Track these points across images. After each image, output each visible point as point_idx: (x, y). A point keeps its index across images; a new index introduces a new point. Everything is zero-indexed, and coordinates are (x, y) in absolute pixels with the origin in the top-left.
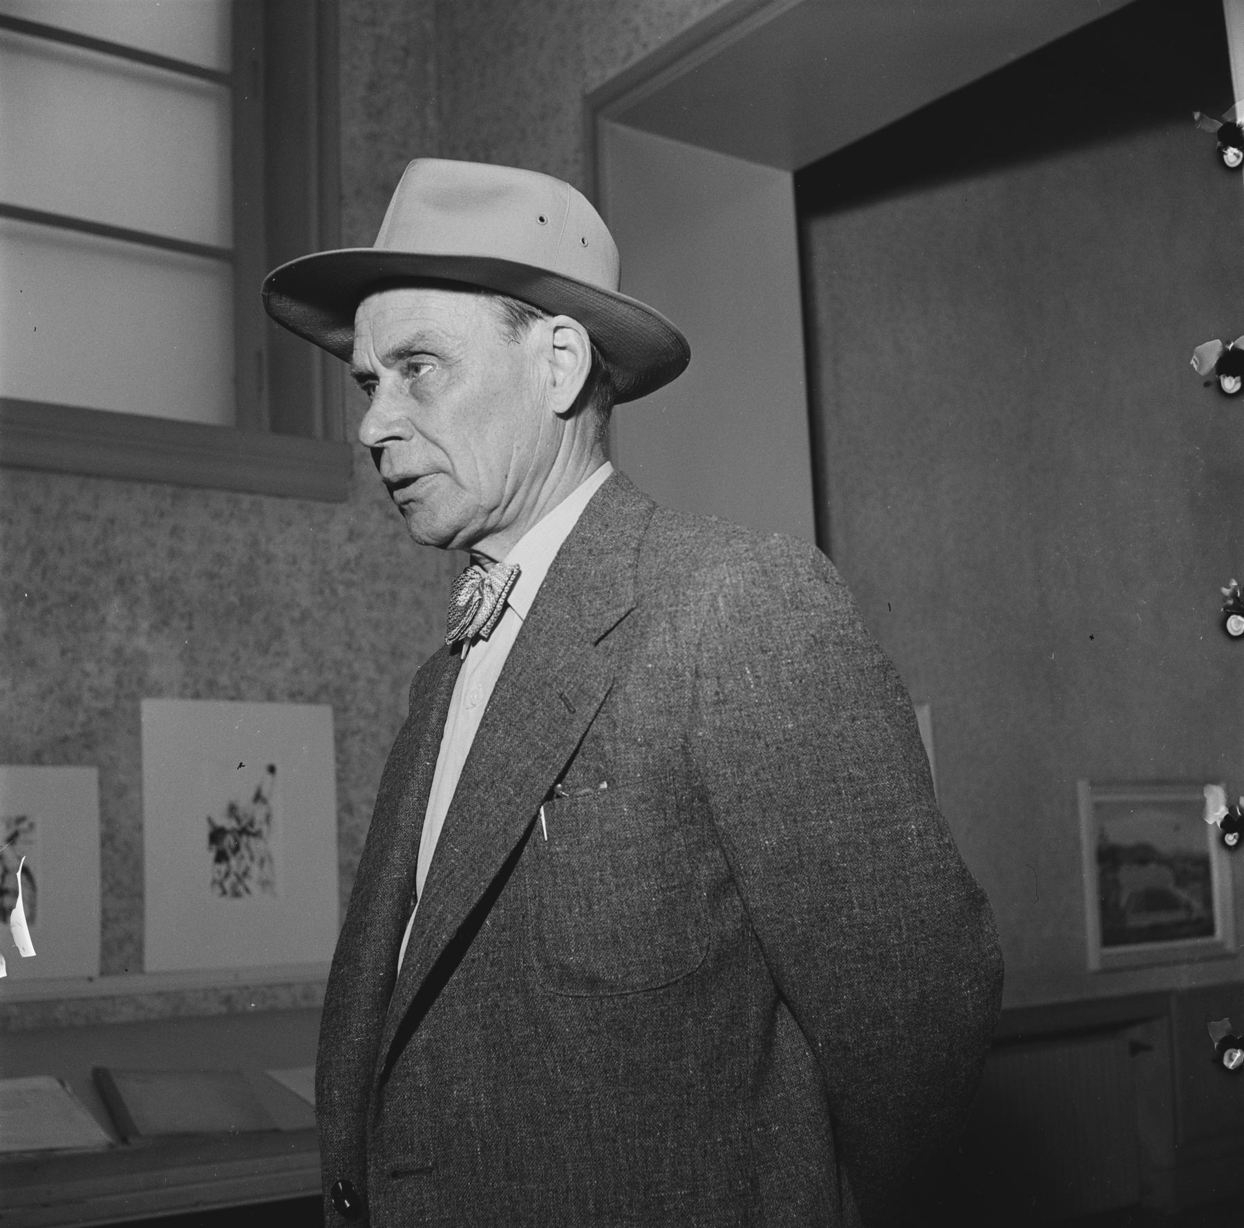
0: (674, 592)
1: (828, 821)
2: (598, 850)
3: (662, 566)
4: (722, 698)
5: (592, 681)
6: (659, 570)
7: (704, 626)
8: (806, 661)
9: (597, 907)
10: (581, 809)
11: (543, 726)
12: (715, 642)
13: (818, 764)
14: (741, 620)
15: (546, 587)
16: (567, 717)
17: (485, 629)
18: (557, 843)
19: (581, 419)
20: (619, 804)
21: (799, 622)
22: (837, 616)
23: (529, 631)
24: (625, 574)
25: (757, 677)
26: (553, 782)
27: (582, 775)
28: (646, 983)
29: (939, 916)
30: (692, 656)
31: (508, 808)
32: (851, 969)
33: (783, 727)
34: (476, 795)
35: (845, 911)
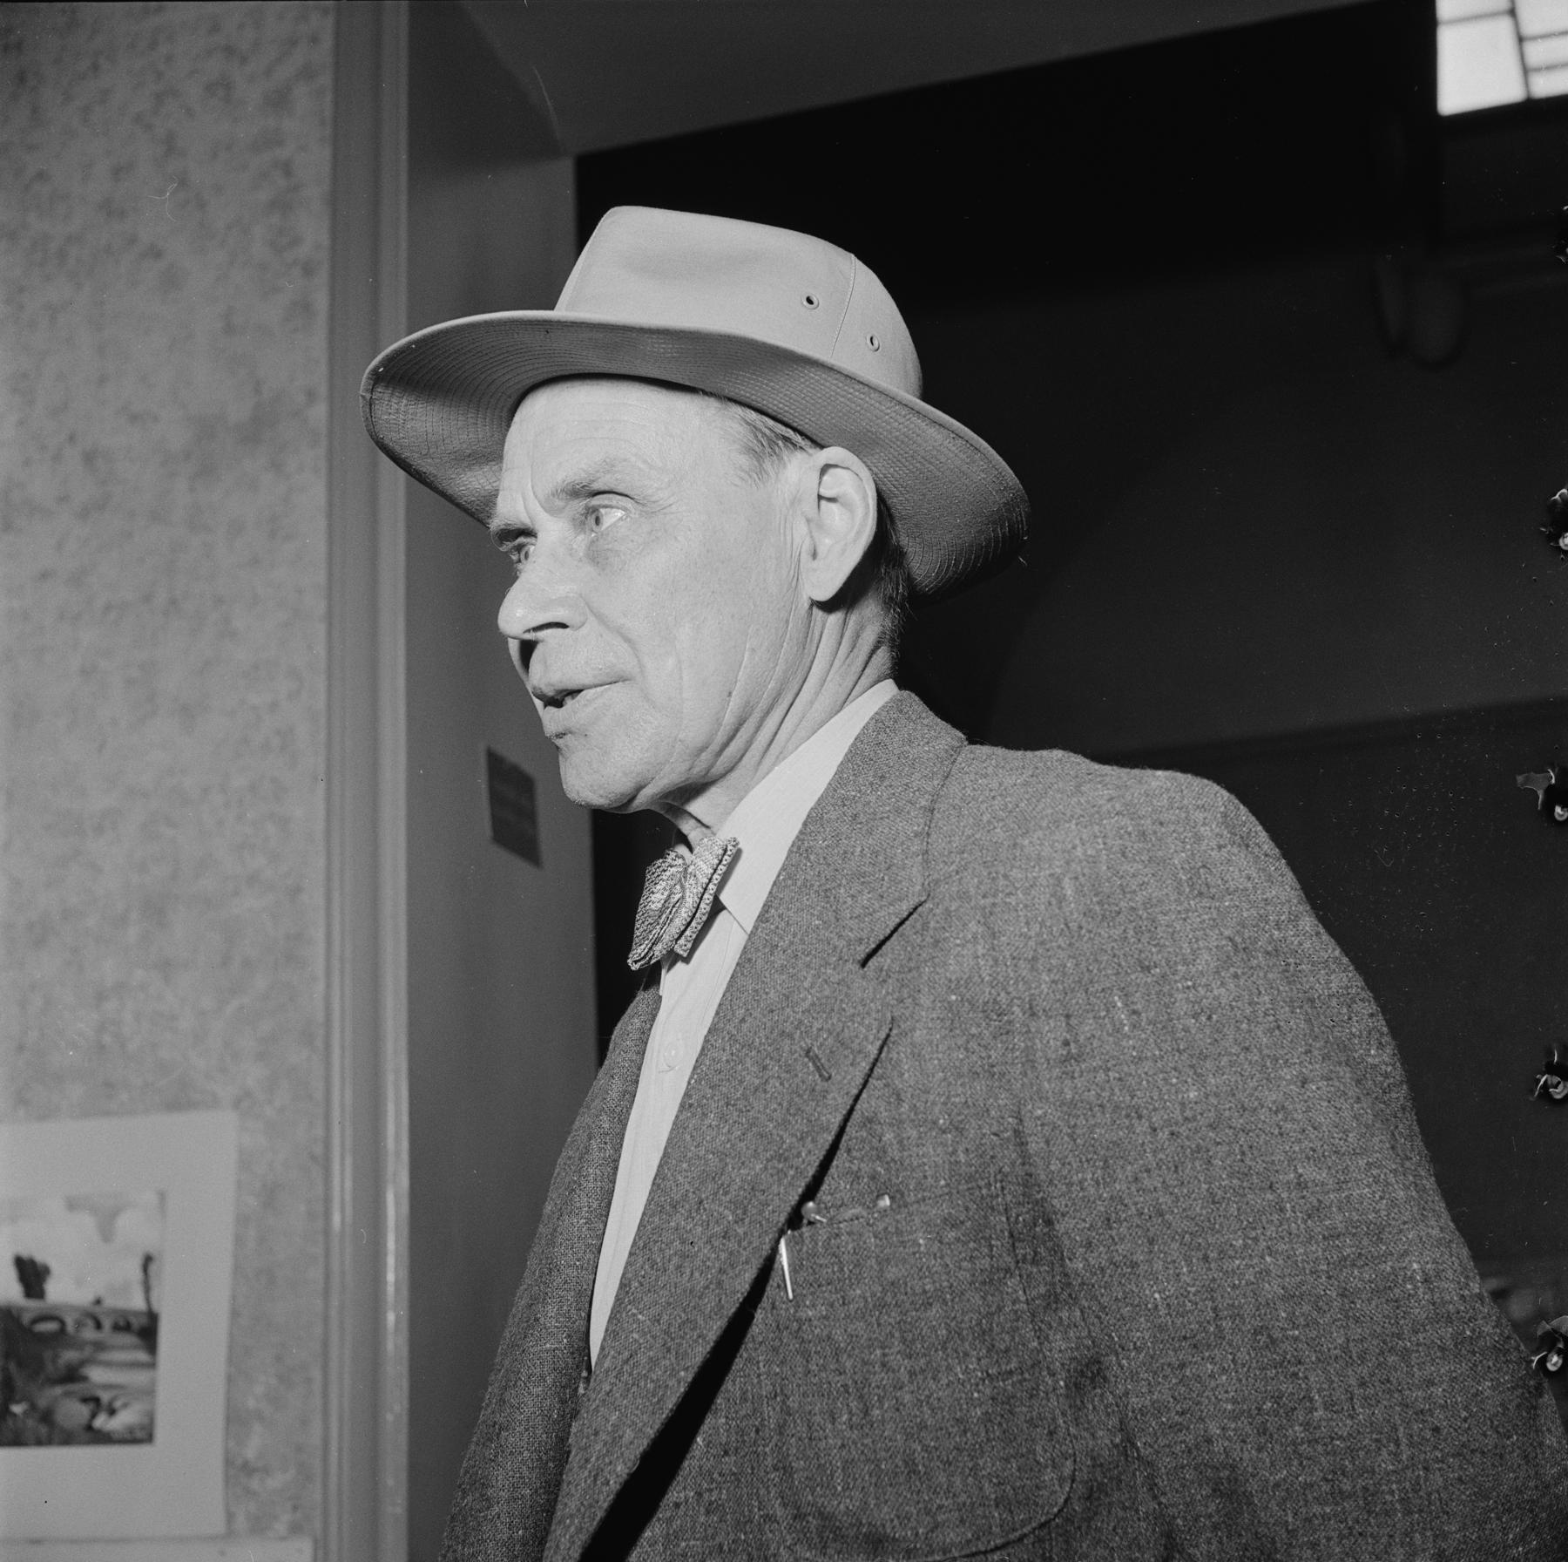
0: (990, 873)
1: (1263, 1258)
2: (877, 1313)
3: (969, 832)
4: (1073, 1051)
5: (856, 1025)
6: (964, 838)
7: (1041, 928)
8: (1219, 983)
9: (878, 1412)
10: (847, 1243)
11: (780, 1104)
12: (1062, 954)
13: (1242, 1161)
14: (1103, 916)
15: (784, 880)
16: (818, 1088)
17: (682, 941)
18: (808, 1303)
19: (854, 618)
20: (910, 1233)
21: (1206, 917)
22: (1269, 908)
23: (757, 950)
24: (908, 848)
25: (1134, 1012)
26: (797, 1198)
27: (848, 1187)
28: (969, 1542)
29: (1465, 1420)
30: (1023, 979)
31: (724, 1245)
32: (1314, 1515)
33: (1180, 1096)
34: (673, 1224)
35: (1300, 1415)
